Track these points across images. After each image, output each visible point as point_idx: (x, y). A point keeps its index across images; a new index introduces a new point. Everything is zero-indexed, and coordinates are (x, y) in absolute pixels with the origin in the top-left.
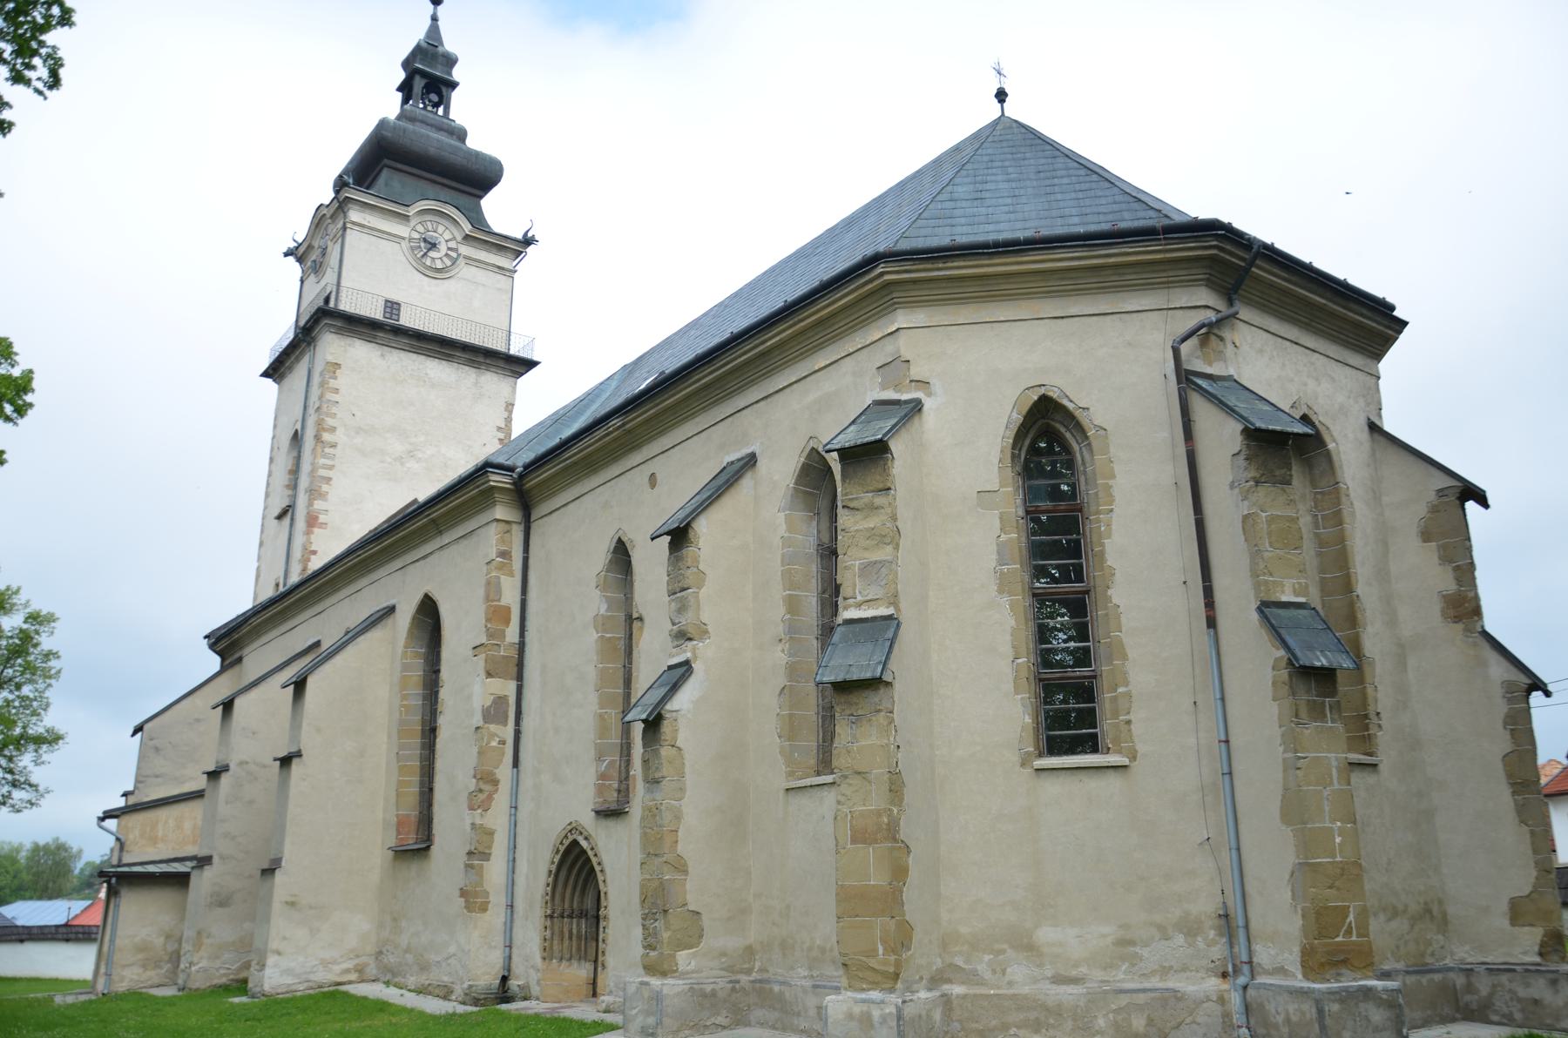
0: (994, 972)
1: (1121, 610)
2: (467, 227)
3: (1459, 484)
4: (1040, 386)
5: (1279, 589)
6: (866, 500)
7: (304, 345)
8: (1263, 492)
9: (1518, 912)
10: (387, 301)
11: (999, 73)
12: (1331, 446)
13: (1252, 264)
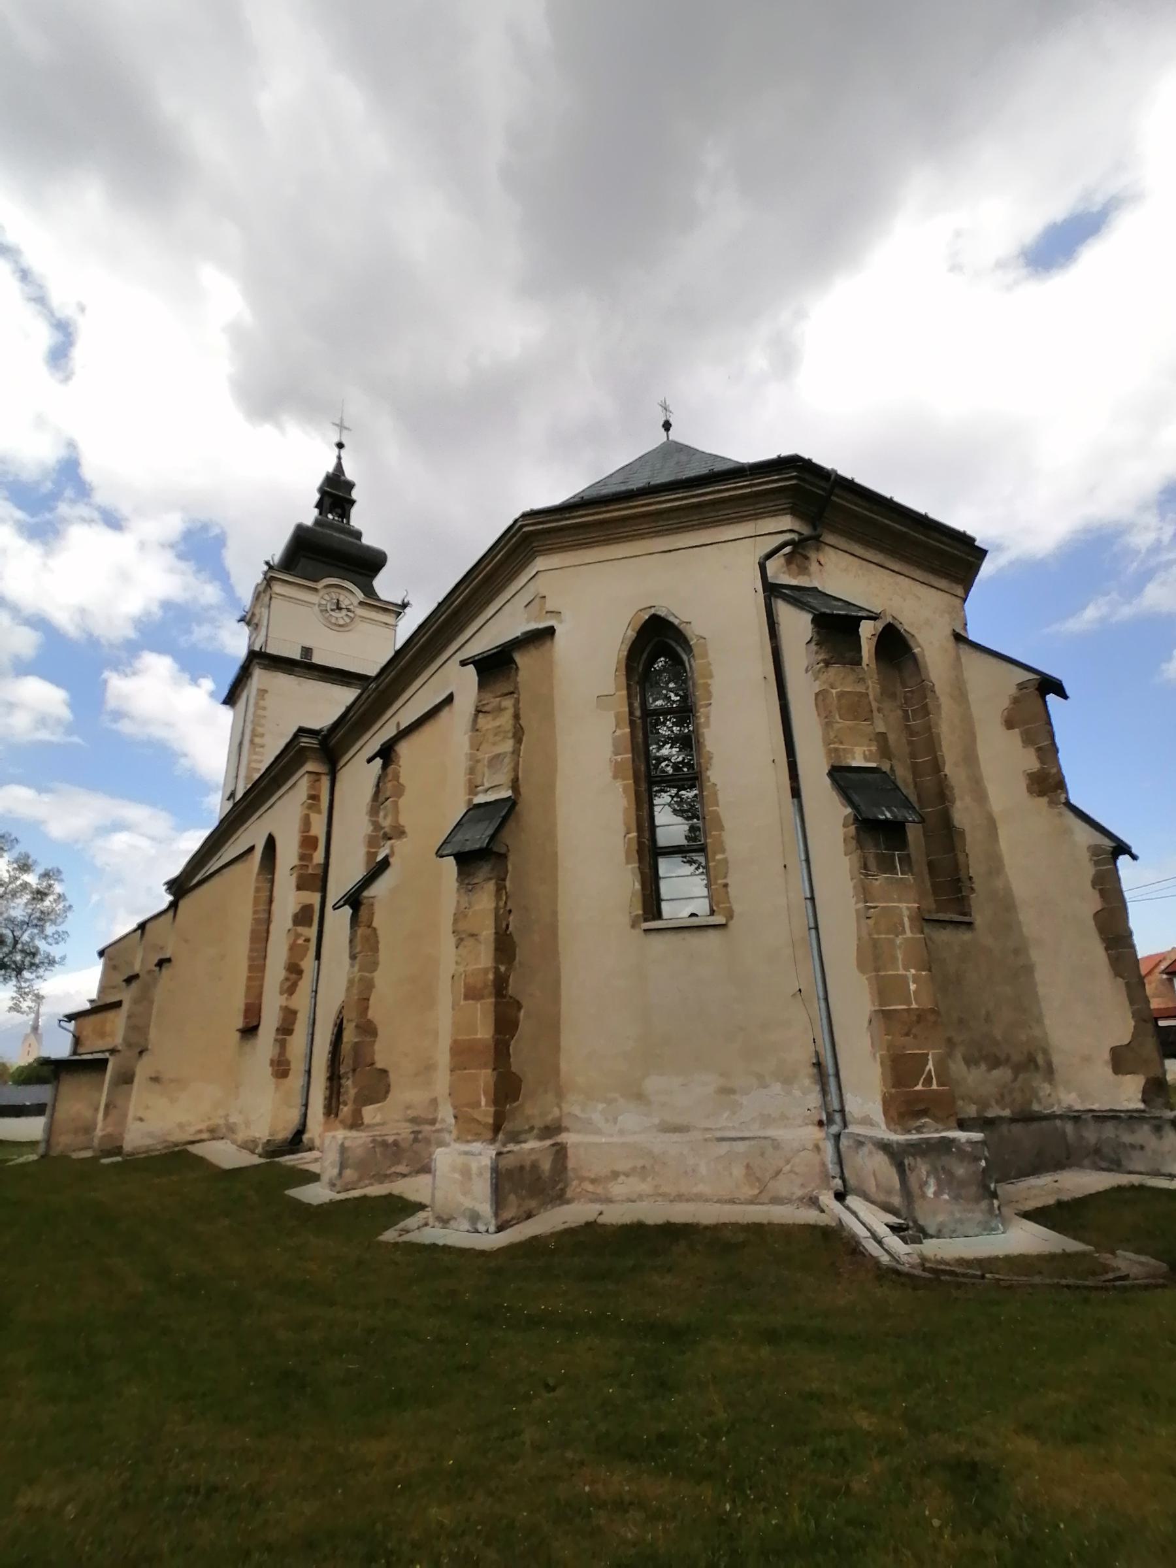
0: (607, 1120)
1: (718, 788)
2: (361, 596)
3: (1038, 677)
4: (651, 607)
5: (849, 756)
6: (494, 704)
7: (245, 679)
8: (834, 670)
9: (1120, 1061)
10: (303, 647)
11: (666, 409)
12: (916, 650)
13: (831, 493)
